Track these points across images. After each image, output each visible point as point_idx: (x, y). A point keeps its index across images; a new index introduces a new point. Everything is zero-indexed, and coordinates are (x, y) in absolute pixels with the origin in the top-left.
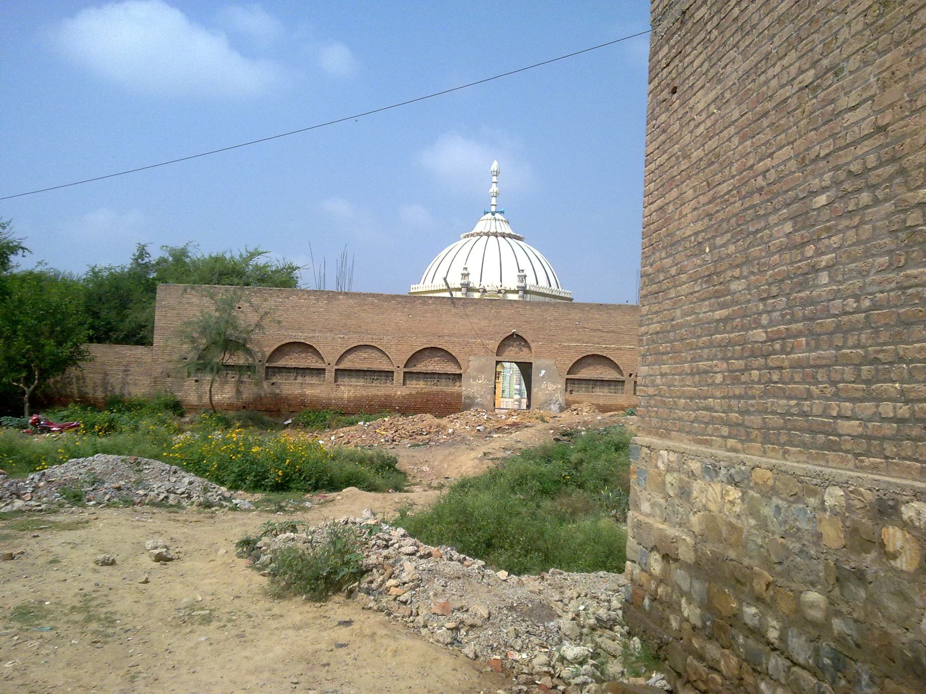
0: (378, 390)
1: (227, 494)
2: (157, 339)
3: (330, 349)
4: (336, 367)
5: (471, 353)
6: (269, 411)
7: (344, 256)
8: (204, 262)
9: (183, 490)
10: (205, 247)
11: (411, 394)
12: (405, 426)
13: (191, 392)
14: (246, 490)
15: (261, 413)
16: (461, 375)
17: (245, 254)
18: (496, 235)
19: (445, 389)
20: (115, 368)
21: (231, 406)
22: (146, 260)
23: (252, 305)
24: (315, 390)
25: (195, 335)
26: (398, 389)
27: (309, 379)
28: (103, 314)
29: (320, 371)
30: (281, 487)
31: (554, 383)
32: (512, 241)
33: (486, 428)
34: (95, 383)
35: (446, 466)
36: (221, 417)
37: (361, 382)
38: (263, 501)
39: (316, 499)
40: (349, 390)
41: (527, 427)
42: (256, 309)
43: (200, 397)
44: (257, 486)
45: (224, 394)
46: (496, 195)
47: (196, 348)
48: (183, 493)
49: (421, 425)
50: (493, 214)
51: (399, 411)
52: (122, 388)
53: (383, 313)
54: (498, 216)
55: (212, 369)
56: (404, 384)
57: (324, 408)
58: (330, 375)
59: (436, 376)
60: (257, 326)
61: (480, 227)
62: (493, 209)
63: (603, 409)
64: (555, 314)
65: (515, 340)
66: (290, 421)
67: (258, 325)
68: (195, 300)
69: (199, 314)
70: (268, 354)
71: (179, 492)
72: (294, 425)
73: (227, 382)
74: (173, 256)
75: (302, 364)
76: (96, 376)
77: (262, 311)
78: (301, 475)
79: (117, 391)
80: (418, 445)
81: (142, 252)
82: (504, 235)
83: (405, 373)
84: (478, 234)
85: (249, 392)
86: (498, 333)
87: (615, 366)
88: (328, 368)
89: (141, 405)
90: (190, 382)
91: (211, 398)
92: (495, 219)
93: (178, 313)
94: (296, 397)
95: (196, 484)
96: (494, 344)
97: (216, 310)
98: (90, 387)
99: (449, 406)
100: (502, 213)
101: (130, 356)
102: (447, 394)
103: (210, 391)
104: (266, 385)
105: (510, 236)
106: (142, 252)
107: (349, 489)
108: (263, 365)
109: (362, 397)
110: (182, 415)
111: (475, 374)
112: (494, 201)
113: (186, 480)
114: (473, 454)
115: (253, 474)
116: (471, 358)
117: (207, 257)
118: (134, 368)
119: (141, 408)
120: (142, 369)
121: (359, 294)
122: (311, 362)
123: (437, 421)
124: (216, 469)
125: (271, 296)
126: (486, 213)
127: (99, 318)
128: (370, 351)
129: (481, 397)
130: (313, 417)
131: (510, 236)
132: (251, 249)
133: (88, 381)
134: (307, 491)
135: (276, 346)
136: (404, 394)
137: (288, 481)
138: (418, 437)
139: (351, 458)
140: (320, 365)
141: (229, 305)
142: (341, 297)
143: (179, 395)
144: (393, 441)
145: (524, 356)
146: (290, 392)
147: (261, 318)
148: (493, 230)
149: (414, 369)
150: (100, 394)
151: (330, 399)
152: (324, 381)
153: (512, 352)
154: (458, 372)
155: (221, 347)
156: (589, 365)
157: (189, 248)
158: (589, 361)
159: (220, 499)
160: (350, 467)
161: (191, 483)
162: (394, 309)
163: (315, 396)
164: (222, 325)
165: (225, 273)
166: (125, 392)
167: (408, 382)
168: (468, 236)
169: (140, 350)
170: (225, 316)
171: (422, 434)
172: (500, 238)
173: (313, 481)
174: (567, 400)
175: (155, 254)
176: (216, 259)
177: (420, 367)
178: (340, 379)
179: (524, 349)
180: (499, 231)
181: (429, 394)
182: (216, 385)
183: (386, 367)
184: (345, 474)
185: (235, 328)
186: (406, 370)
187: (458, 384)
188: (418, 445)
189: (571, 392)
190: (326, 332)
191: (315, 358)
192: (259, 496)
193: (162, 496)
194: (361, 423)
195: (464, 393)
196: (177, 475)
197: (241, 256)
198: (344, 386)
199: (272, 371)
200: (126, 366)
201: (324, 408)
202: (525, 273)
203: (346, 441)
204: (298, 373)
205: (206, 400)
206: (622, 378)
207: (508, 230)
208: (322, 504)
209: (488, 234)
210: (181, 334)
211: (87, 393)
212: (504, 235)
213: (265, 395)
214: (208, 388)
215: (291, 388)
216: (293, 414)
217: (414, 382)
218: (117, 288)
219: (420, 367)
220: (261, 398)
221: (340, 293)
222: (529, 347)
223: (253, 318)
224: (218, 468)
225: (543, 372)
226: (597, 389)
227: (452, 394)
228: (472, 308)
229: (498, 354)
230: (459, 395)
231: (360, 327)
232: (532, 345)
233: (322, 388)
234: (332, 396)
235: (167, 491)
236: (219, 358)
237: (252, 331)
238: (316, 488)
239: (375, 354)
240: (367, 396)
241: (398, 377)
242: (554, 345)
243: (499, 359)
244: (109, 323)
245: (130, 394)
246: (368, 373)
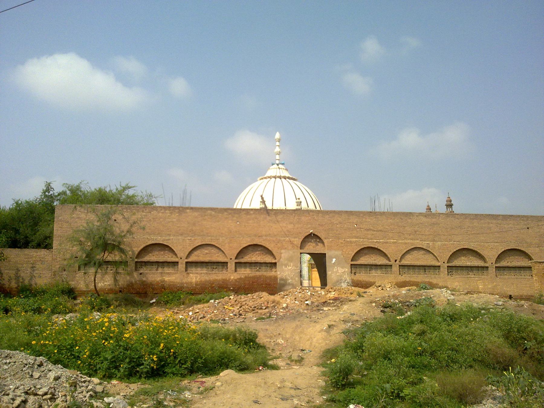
0: (217, 276)
1: (99, 389)
2: (55, 244)
3: (182, 247)
4: (186, 260)
5: (282, 248)
6: (138, 293)
7: (185, 192)
8: (92, 194)
9: (45, 390)
10: (91, 184)
11: (241, 279)
12: (248, 303)
13: (81, 281)
14: (121, 379)
15: (133, 295)
16: (275, 264)
17: (119, 188)
18: (280, 177)
19: (265, 274)
20: (25, 265)
21: (111, 291)
22: (51, 192)
23: (124, 218)
24: (171, 277)
25: (82, 239)
26: (232, 275)
27: (166, 270)
28: (21, 230)
29: (175, 264)
30: (157, 373)
31: (342, 268)
32: (291, 181)
33: (312, 303)
34: (10, 277)
35: (297, 338)
36: (101, 301)
37: (204, 271)
38: (138, 394)
39: (195, 386)
40: (196, 277)
41: (351, 301)
42: (127, 220)
43: (87, 286)
44: (131, 374)
45: (106, 282)
46: (279, 153)
47: (82, 249)
48: (46, 394)
49: (259, 301)
50: (278, 165)
51: (233, 291)
52: (30, 279)
53: (218, 221)
54: (280, 166)
55: (95, 264)
56: (236, 271)
57: (178, 290)
58: (182, 266)
59: (258, 265)
60: (128, 232)
61: (269, 173)
62: (277, 162)
63: (401, 285)
64: (340, 219)
65: (312, 238)
66: (154, 301)
67: (128, 231)
68: (83, 216)
69: (85, 225)
70: (137, 253)
71: (40, 392)
72: (158, 303)
73: (106, 273)
74: (72, 191)
75: (161, 259)
76: (10, 272)
77: (131, 222)
78: (175, 358)
79: (26, 282)
80: (263, 319)
81: (48, 188)
82: (285, 178)
83: (236, 263)
84: (269, 177)
85: (124, 280)
86: (300, 233)
87: (385, 255)
88: (180, 261)
89: (44, 292)
90: (80, 274)
91: (95, 286)
92: (279, 168)
93: (69, 225)
94: (158, 283)
95: (63, 379)
96: (298, 241)
97: (98, 221)
98: (6, 279)
99: (273, 287)
100: (283, 164)
101: (36, 257)
102: (266, 277)
103: (95, 280)
104: (135, 274)
105: (289, 178)
106: (48, 188)
107: (226, 372)
108: (133, 260)
109: (206, 281)
110: (75, 298)
111: (286, 262)
112: (277, 157)
113: (52, 375)
114: (318, 327)
115: (127, 360)
116: (283, 251)
117: (93, 190)
118: (38, 266)
119: (44, 294)
120: (45, 266)
121: (201, 209)
122: (168, 257)
123: (272, 297)
124: (88, 356)
125: (138, 211)
126: (273, 164)
127: (19, 234)
128: (210, 248)
129: (292, 278)
130: (171, 297)
131: (289, 178)
132: (124, 185)
133: (4, 275)
134: (183, 376)
135: (142, 247)
136: (236, 278)
137: (163, 366)
138: (260, 311)
139: (216, 336)
140: (174, 259)
141: (108, 217)
142: (188, 211)
143: (73, 284)
144: (240, 315)
145: (319, 249)
146: (153, 279)
147: (131, 226)
148: (278, 175)
149: (242, 260)
150: (14, 285)
151: (183, 283)
152: (178, 271)
153: (312, 247)
154: (274, 261)
155: (102, 248)
156: (366, 254)
157: (82, 186)
158: (366, 251)
159: (91, 396)
160: (220, 346)
161: (57, 379)
162: (226, 218)
163: (172, 282)
164: (102, 231)
165: (103, 198)
166: (33, 283)
167: (238, 270)
168: (262, 179)
169: (42, 253)
170: (104, 225)
171: (261, 309)
172: (283, 179)
173: (189, 364)
174: (352, 280)
175: (58, 188)
176: (100, 191)
177: (247, 259)
178: (189, 269)
179: (319, 244)
180: (282, 175)
181: (254, 277)
182: (98, 276)
183: (222, 259)
184: (217, 354)
185: (112, 234)
186: (237, 261)
187: (274, 270)
188: (263, 319)
189: (355, 273)
190: (178, 236)
191: (171, 255)
192: (135, 387)
193: (18, 402)
194: (212, 301)
195: (279, 276)
196: (42, 369)
197: (117, 189)
198: (192, 273)
199: (140, 265)
200: (33, 264)
201: (178, 290)
202: (301, 200)
203: (202, 316)
204: (158, 266)
205: (92, 287)
206: (390, 263)
207: (287, 174)
208: (201, 393)
209: (275, 177)
210: (72, 239)
211: (4, 284)
212: (285, 178)
213: (136, 282)
214: (93, 278)
215: (154, 276)
216: (156, 295)
217: (243, 269)
218: (31, 212)
219: (247, 259)
220: (132, 283)
221: (187, 208)
222: (323, 243)
223: (125, 227)
224: (90, 357)
225: (334, 260)
226: (373, 271)
227: (271, 277)
228: (281, 216)
229: (301, 248)
230: (276, 278)
231: (202, 231)
232: (325, 241)
233: (177, 275)
234: (184, 281)
235: (26, 393)
236: (99, 256)
237: (125, 236)
238: (192, 371)
239: (214, 250)
240: (210, 280)
241: (231, 266)
242: (340, 241)
243: (302, 251)
244: (26, 237)
245: (36, 284)
246: (210, 264)
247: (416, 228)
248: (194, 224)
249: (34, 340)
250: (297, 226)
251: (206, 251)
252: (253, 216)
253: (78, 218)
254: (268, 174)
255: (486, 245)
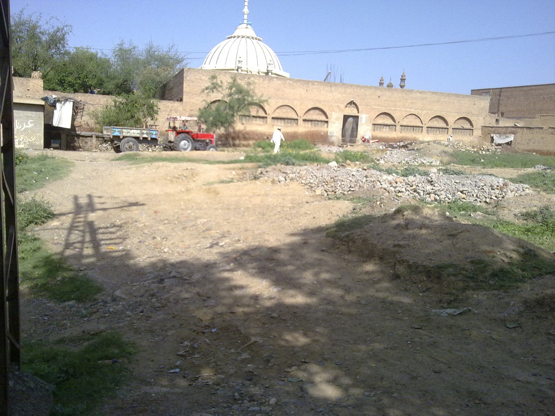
5: (333, 110)
116: (333, 113)
154: (327, 120)
169: (176, 104)
239: (290, 110)
247: (414, 101)
248: (278, 90)
249: (217, 370)
250: (343, 95)
251: (285, 110)
252: (317, 86)
253: (201, 79)
254: (236, 33)
255: (450, 114)
